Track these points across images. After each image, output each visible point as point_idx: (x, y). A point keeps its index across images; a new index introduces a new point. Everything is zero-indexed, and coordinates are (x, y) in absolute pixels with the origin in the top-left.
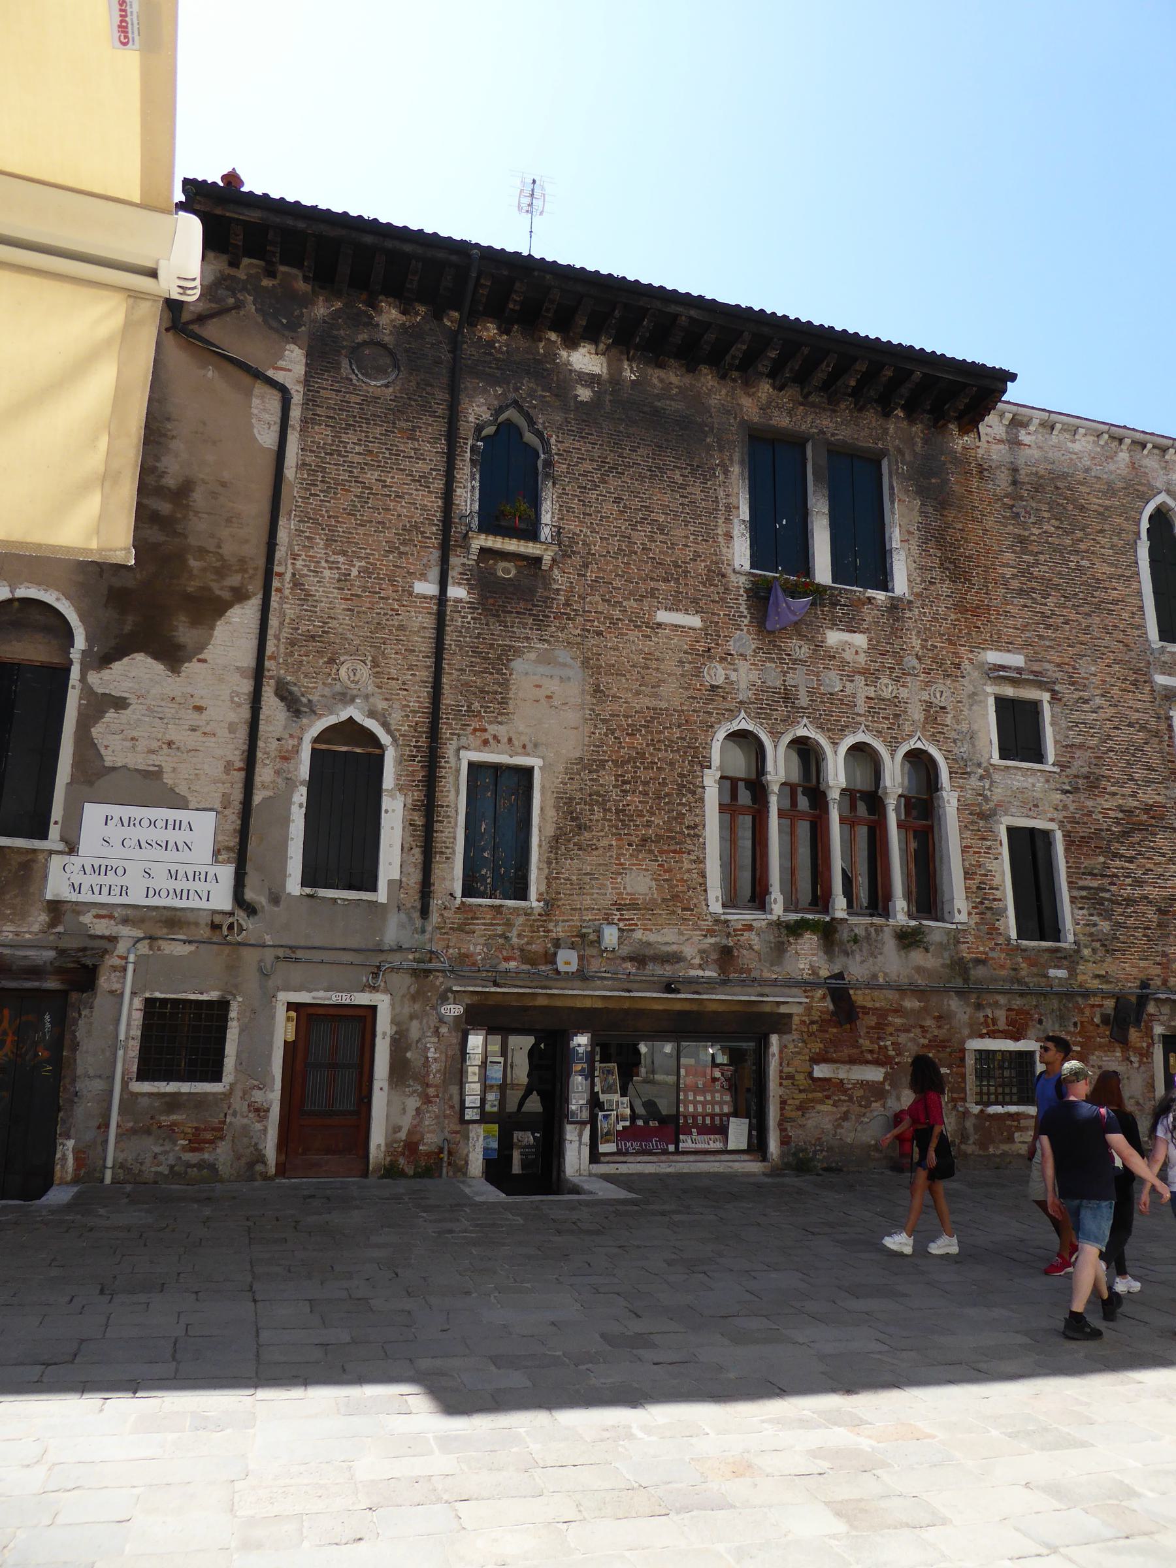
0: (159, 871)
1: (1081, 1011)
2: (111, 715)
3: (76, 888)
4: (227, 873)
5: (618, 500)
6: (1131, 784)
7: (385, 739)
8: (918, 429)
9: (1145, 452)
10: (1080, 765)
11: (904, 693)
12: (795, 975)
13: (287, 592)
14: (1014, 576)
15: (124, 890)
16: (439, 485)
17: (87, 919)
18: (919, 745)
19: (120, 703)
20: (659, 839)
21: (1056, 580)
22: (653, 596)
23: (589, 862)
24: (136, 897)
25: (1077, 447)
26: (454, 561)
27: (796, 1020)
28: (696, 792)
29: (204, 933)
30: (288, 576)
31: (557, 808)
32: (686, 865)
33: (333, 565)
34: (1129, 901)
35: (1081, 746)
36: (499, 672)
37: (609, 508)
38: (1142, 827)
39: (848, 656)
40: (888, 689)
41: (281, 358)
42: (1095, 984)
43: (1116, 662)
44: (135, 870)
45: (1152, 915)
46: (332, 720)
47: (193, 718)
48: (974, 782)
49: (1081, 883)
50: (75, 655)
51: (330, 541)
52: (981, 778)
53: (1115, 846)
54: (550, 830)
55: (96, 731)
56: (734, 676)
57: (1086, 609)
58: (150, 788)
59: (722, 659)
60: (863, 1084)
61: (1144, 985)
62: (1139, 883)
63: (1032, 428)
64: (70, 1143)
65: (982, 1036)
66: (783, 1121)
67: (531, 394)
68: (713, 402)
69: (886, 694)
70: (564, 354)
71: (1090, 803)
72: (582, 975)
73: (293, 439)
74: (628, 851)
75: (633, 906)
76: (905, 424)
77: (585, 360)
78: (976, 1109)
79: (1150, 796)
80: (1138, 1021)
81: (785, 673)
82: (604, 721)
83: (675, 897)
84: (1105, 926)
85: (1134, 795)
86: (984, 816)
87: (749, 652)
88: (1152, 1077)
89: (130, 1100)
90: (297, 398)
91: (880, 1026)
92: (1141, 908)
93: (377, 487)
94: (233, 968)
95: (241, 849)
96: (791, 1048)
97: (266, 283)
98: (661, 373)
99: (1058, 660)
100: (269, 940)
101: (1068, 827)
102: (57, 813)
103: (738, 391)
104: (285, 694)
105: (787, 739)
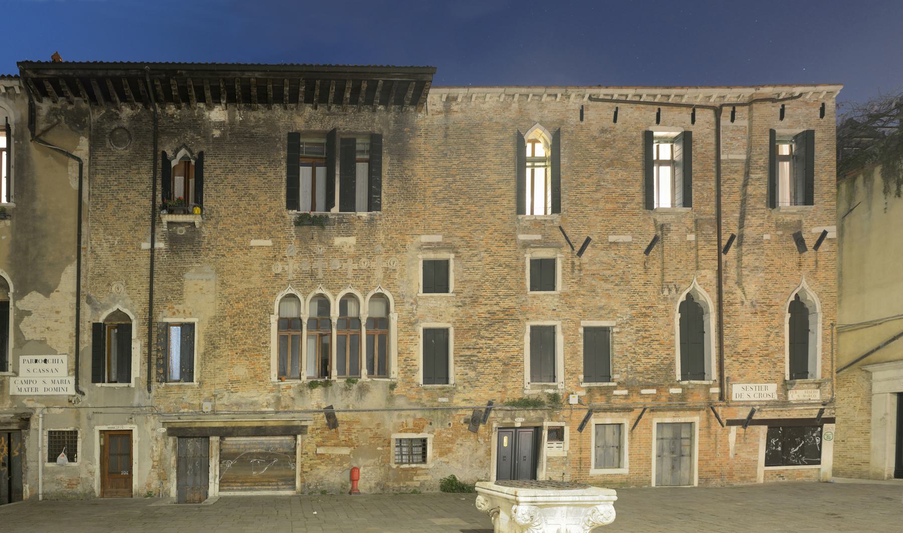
0: (48, 380)
1: (454, 417)
2: (26, 318)
3: (20, 390)
4: (72, 379)
5: (233, 187)
6: (497, 298)
7: (132, 317)
8: (391, 116)
9: (529, 100)
10: (468, 291)
11: (373, 265)
12: (310, 408)
13: (89, 256)
14: (441, 191)
15: (36, 390)
16: (150, 194)
17: (25, 402)
18: (380, 291)
19: (29, 313)
20: (249, 350)
21: (465, 189)
22: (249, 233)
23: (219, 363)
24: (41, 392)
25: (486, 106)
26: (157, 230)
27: (310, 428)
28: (266, 326)
29: (67, 404)
30: (89, 249)
31: (205, 340)
32: (262, 361)
33: (107, 241)
34: (487, 361)
35: (470, 281)
36: (179, 280)
37: (229, 191)
38: (501, 321)
39: (345, 249)
40: (364, 263)
41: (78, 144)
42: (463, 404)
43: (496, 231)
44: (40, 381)
45: (500, 367)
46: (110, 311)
47: (55, 316)
48: (407, 307)
49: (461, 354)
50: (10, 295)
51: (106, 229)
52: (412, 304)
53: (483, 333)
54: (202, 350)
55: (21, 326)
56: (286, 268)
57: (482, 202)
58: (43, 347)
59: (282, 260)
60: (340, 456)
61: (490, 403)
62: (494, 351)
63: (459, 100)
64: (27, 486)
65: (401, 432)
66: (303, 472)
67: (192, 139)
68: (281, 124)
69: (364, 267)
70: (207, 113)
71: (471, 311)
72: (214, 412)
73: (85, 183)
74: (235, 356)
75: (238, 381)
76: (384, 114)
77: (218, 114)
78: (394, 466)
79: (507, 303)
80: (484, 421)
81: (312, 263)
82: (226, 297)
83: (256, 376)
84: (472, 374)
85: (497, 304)
86: (412, 324)
87: (294, 254)
88: (490, 450)
89: (45, 470)
90: (86, 164)
91: (349, 430)
92: (494, 364)
93: (124, 201)
94: (78, 417)
95: (76, 372)
96: (307, 441)
97: (70, 108)
98: (255, 113)
99: (462, 235)
100: (90, 405)
101: (458, 325)
102: (10, 360)
103: (295, 115)
104: (89, 300)
105: (311, 296)
